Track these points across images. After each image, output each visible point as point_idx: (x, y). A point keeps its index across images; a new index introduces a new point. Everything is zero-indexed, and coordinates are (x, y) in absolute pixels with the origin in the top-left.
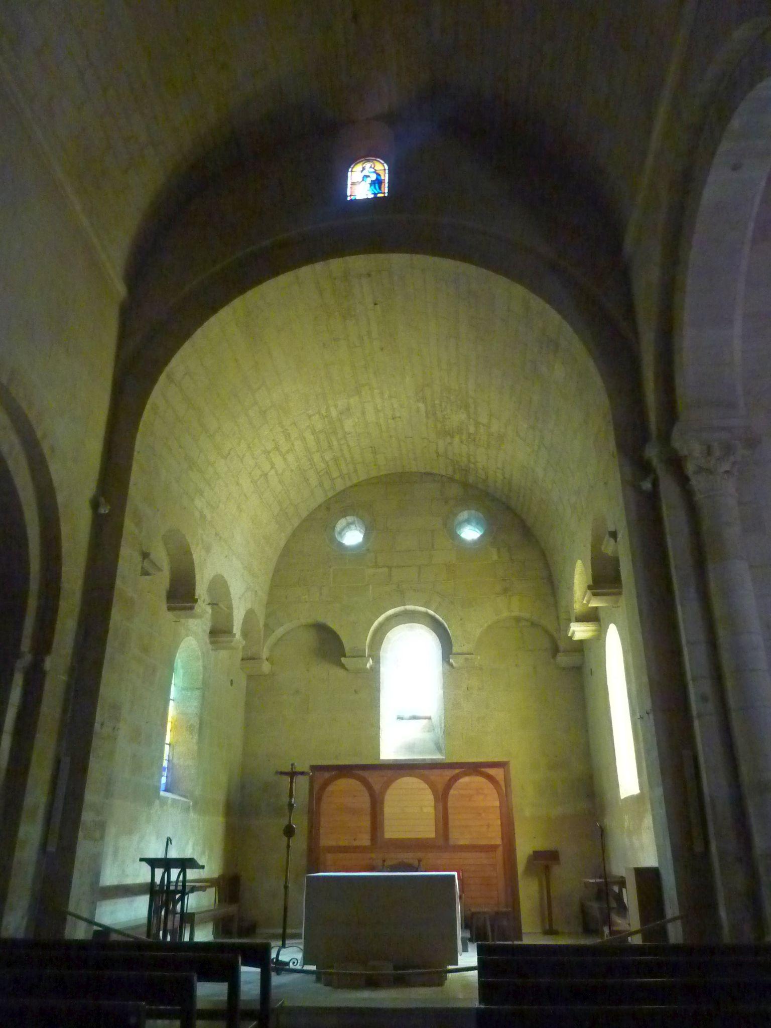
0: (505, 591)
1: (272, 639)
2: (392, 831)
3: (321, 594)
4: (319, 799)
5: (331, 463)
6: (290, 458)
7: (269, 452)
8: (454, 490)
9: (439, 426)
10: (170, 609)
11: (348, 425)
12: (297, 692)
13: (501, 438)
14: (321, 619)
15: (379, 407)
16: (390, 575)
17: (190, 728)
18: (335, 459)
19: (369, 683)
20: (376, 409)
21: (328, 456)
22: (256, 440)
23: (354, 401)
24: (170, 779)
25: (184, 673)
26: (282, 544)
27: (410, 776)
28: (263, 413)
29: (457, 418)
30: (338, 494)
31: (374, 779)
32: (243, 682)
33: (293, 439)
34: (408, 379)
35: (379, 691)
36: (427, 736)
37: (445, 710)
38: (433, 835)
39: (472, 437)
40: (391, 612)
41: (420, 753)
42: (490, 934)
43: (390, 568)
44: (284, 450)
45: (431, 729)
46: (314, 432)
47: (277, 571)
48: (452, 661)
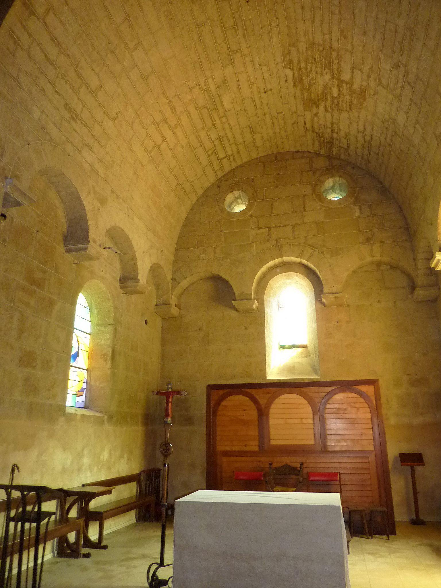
0: (368, 240)
1: (178, 290)
2: (277, 438)
3: (215, 252)
4: (215, 412)
5: (217, 142)
6: (179, 132)
7: (158, 124)
8: (321, 163)
9: (306, 95)
10: (68, 251)
11: (227, 99)
12: (200, 329)
13: (363, 93)
14: (216, 271)
15: (252, 79)
16: (270, 235)
17: (104, 356)
18: (220, 139)
19: (256, 321)
20: (249, 81)
21: (213, 135)
22: (143, 109)
23: (229, 71)
24: (88, 398)
25: (98, 312)
26: (184, 216)
27: (291, 392)
28: (145, 78)
29: (323, 80)
30: (227, 174)
31: (262, 397)
32: (159, 322)
33: (178, 113)
34: (275, 39)
35: (264, 326)
36: (304, 360)
37: (319, 343)
38: (312, 442)
39: (336, 101)
40: (271, 263)
41: (300, 374)
42: (367, 530)
43: (269, 229)
44: (172, 124)
45: (307, 355)
46: (197, 108)
47: (180, 237)
48: (323, 300)
